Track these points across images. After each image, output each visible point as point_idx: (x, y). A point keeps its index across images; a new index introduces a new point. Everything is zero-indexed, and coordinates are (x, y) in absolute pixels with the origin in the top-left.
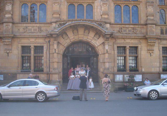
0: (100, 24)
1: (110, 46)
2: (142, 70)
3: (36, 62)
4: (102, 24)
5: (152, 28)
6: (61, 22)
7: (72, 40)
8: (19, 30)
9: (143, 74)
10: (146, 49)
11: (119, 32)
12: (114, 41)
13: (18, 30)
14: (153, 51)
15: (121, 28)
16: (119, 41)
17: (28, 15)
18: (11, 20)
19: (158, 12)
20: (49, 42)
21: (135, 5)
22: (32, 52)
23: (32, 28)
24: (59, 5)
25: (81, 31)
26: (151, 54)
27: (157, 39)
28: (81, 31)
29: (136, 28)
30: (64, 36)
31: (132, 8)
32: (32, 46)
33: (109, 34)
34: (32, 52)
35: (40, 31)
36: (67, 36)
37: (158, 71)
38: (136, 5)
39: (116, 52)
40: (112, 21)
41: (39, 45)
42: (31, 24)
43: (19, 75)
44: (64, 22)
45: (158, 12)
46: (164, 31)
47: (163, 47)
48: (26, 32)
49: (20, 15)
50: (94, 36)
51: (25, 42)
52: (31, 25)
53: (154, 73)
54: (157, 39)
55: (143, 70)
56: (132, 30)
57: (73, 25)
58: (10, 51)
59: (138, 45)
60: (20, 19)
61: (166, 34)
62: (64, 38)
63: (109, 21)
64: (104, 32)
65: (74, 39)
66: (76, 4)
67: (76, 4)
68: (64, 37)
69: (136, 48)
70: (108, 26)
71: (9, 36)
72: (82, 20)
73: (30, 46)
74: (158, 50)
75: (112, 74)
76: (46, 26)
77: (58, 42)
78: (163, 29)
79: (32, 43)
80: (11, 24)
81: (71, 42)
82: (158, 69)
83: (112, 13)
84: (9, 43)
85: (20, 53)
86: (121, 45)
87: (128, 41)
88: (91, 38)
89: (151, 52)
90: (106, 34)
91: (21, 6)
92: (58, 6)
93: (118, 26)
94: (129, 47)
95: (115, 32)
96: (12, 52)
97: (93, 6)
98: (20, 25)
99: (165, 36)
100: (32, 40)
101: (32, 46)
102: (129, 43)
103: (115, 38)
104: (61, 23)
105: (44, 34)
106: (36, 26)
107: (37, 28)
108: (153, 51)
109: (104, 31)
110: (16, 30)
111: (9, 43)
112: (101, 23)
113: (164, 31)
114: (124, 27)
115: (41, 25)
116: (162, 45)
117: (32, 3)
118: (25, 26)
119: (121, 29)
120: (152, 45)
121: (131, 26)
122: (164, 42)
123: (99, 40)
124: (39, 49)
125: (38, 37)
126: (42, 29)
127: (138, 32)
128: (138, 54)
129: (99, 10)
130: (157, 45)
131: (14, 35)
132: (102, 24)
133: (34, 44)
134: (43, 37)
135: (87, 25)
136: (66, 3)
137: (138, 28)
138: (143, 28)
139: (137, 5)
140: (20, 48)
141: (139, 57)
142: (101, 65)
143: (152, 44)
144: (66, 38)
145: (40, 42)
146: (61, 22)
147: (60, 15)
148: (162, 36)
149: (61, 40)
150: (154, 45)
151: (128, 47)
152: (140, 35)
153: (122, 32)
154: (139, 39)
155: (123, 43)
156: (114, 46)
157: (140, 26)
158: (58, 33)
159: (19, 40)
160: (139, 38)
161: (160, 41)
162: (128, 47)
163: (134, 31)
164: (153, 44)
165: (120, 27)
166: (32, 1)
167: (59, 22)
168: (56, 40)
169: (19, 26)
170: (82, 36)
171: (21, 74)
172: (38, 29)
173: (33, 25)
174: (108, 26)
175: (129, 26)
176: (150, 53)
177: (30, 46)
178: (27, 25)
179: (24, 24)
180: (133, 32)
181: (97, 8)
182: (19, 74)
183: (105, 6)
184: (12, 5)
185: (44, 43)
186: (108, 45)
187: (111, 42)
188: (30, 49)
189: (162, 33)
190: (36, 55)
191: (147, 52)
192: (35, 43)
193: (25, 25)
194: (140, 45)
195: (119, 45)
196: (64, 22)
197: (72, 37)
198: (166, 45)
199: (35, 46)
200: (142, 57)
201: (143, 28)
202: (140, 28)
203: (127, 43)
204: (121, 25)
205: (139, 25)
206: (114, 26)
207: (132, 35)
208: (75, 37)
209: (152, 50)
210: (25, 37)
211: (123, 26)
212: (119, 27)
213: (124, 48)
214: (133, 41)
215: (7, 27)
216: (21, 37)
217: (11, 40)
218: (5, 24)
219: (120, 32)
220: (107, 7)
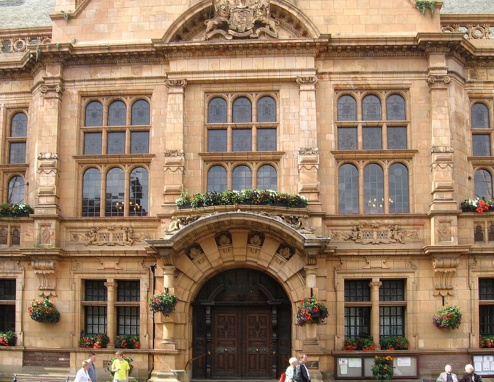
0: (294, 217)
1: (322, 279)
2: (417, 344)
3: (45, 354)
4: (299, 217)
5: (448, 224)
6: (183, 216)
7: (215, 265)
8: (75, 237)
9: (417, 356)
10: (431, 287)
11: (351, 238)
12: (336, 264)
13: (74, 237)
14: (450, 292)
15: (355, 228)
16: (350, 265)
17: (99, 199)
18: (54, 212)
19: (470, 178)
20: (153, 268)
21: (397, 160)
22: (110, 295)
23: (110, 232)
24: (182, 168)
25: (239, 242)
26: (445, 299)
27: (462, 255)
28: (239, 242)
29: (402, 227)
30: (193, 252)
31: (389, 169)
32: (110, 279)
33: (315, 244)
34: (110, 295)
35: (129, 239)
36: (202, 252)
37: (466, 345)
38: (401, 160)
39: (341, 295)
40: (331, 210)
41: (127, 277)
42: (106, 221)
43: (76, 356)
44: (193, 216)
45: (470, 178)
46: (486, 230)
47: (481, 280)
48: (93, 243)
49: (80, 198)
50: (278, 252)
51: (92, 270)
52: (108, 224)
53: (454, 353)
54: (462, 255)
55: (422, 344)
56: (390, 234)
57: (216, 223)
58: (53, 293)
59: (407, 274)
60: (77, 208)
61: (490, 239)
62: (192, 259)
63: (321, 211)
64: (300, 241)
65: (221, 262)
66: (229, 164)
67: (229, 164)
68: (192, 256)
69: (402, 282)
70: (318, 222)
71: (48, 253)
72: (242, 210)
73: (105, 281)
74: (465, 286)
75: (328, 355)
76: (148, 228)
77: (177, 269)
78: (482, 225)
79: (110, 273)
80: (53, 223)
81: (212, 270)
82: (466, 340)
83: (331, 189)
84: (49, 272)
85: (78, 297)
86: (356, 275)
87: (376, 263)
88: (265, 258)
89: (444, 293)
90: (306, 244)
91: (81, 175)
92: (177, 172)
93: (348, 222)
94: (381, 280)
95: (341, 238)
96: (57, 296)
97: (278, 169)
98: (78, 224)
99: (488, 245)
100: (111, 264)
101: (110, 279)
102: (380, 270)
103: (339, 256)
104: (185, 218)
105: (141, 247)
106: (121, 228)
107: (123, 231)
108: (451, 289)
109: (300, 236)
110: (67, 236)
111: (49, 272)
112: (297, 216)
113: (486, 230)
114: (365, 225)
115: (133, 224)
116: (479, 273)
117: (109, 165)
118: (90, 228)
119: (358, 230)
120: (449, 272)
121: (386, 221)
122: (487, 263)
123: (289, 263)
124: (127, 288)
125: (124, 255)
126: (137, 235)
127: (406, 239)
128: (407, 299)
129: (292, 179)
130: (462, 271)
131: (62, 251)
132: (299, 217)
133: (114, 276)
134: (139, 255)
135: (253, 222)
136: (201, 162)
137: (408, 225)
138: (423, 225)
139: (406, 162)
140: (78, 285)
141: (409, 309)
142: (297, 331)
143: (446, 271)
144: (200, 257)
145: (130, 270)
146: (183, 216)
147: (318, 193)
148: (477, 246)
149: (187, 265)
150: (454, 272)
151: (376, 280)
152: (411, 246)
153: (358, 237)
154: (409, 258)
155: (362, 271)
156: (336, 280)
157: (411, 221)
158: (171, 244)
159: (75, 264)
160: (410, 253)
161: (471, 261)
162: (376, 280)
163: (395, 237)
164: (451, 270)
165: (353, 226)
166: (110, 161)
167: (179, 216)
168: (171, 265)
169: (76, 228)
170: (240, 254)
171: (79, 352)
172: (124, 235)
173: (113, 224)
174: (318, 222)
175: (379, 221)
176: (443, 297)
177: (105, 281)
178: (97, 224)
179: (88, 221)
180: (392, 237)
181: (288, 175)
182: (76, 352)
183: (309, 167)
184: (55, 171)
185: (140, 273)
186: (314, 276)
187: (326, 269)
188: (105, 289)
189: (479, 236)
190: (121, 303)
191: (432, 293)
192: (118, 273)
193: (91, 224)
194: (411, 275)
195: (350, 276)
196: (193, 216)
197: (214, 258)
198: (492, 273)
199: (118, 281)
200: (419, 307)
201: (423, 225)
202: (412, 227)
203: (373, 270)
204: (357, 218)
205: (409, 217)
206: (334, 222)
207: (391, 247)
208: (224, 255)
209: (447, 289)
210: (91, 257)
211: (363, 221)
212: (350, 226)
213: (366, 284)
214: (391, 264)
215: (43, 228)
216: (80, 255)
217: (54, 264)
218: (37, 223)
219: (354, 240)
220: (316, 171)
